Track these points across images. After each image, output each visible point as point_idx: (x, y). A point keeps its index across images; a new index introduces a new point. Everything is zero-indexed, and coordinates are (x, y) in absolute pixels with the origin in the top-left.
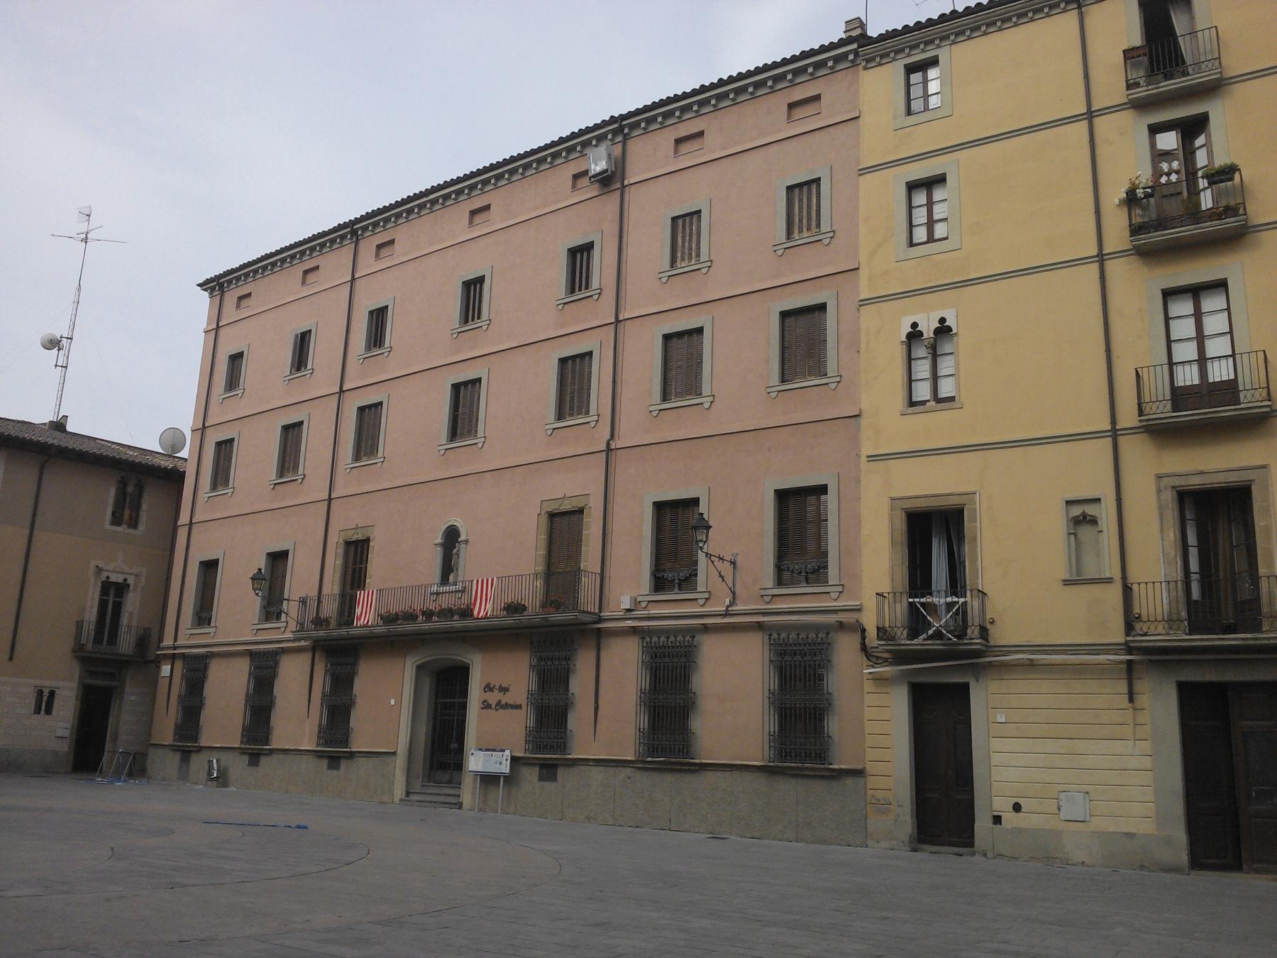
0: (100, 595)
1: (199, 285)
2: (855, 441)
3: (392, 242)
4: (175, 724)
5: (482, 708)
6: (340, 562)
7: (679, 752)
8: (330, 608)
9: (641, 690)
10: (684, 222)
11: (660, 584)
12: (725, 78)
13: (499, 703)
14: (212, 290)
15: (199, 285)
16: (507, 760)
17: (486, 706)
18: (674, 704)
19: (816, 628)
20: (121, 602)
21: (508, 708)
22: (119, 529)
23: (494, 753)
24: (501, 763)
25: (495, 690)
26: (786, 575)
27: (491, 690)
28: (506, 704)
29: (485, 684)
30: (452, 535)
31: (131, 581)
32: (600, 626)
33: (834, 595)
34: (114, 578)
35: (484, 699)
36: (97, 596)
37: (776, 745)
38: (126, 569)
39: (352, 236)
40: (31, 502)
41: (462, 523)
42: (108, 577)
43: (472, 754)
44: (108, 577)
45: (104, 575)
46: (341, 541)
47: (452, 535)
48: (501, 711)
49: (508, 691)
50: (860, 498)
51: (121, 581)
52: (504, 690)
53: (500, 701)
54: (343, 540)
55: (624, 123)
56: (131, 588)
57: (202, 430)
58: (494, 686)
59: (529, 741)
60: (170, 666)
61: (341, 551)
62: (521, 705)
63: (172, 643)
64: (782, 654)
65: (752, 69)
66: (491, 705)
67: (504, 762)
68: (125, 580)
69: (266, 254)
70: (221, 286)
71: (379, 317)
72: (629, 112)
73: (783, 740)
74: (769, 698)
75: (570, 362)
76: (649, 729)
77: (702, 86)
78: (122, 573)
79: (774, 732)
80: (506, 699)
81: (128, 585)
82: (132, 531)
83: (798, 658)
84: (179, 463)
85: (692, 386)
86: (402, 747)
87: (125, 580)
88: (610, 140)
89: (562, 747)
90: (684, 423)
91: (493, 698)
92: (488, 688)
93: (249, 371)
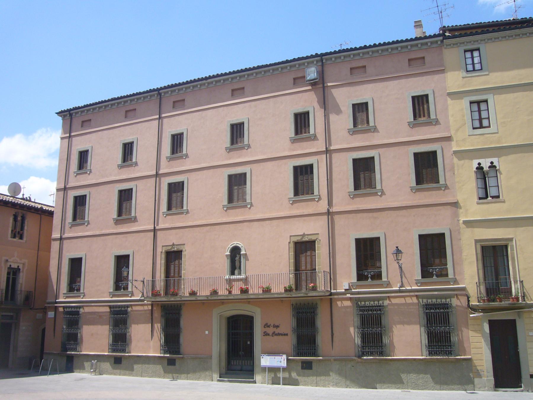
0: (7, 275)
1: (57, 113)
2: (456, 215)
3: (90, 120)
4: (62, 342)
5: (264, 335)
6: (163, 262)
7: (306, 353)
8: (160, 285)
9: (293, 328)
10: (84, 154)
11: (361, 277)
12: (368, 45)
13: (274, 333)
14: (64, 117)
15: (57, 113)
16: (284, 360)
17: (266, 334)
18: (305, 334)
19: (180, 304)
20: (16, 278)
21: (279, 335)
22: (14, 240)
23: (276, 357)
24: (281, 362)
25: (270, 326)
26: (444, 273)
27: (269, 327)
28: (278, 333)
29: (265, 323)
30: (235, 251)
31: (21, 267)
32: (56, 305)
33: (82, 297)
34: (14, 266)
35: (265, 331)
36: (6, 276)
37: (111, 347)
38: (19, 261)
39: (157, 95)
40: (445, 162)
41: (243, 245)
42: (10, 265)
43: (262, 358)
44: (10, 265)
45: (9, 264)
46: (164, 251)
47: (235, 251)
48: (275, 337)
49: (279, 327)
50: (460, 239)
51: (16, 267)
52: (277, 327)
53: (275, 332)
54: (165, 251)
55: (323, 57)
56: (21, 270)
57: (64, 190)
58: (270, 325)
59: (110, 348)
60: (53, 313)
61: (163, 256)
62: (287, 334)
63: (54, 300)
64: (298, 313)
65: (353, 48)
66: (269, 334)
67: (283, 361)
68: (18, 266)
69: (140, 92)
70: (71, 115)
71: (83, 156)
72: (326, 53)
73: (299, 348)
74: (293, 331)
75: (123, 192)
76: (164, 342)
77: (179, 83)
78: (17, 263)
79: (295, 345)
80: (277, 331)
81: (20, 269)
82: (20, 240)
83: (304, 314)
84: (43, 207)
85: (371, 184)
86: (215, 353)
87: (18, 266)
88: (315, 64)
89: (178, 352)
90: (79, 231)
91: (270, 330)
92: (267, 326)
93: (93, 162)
